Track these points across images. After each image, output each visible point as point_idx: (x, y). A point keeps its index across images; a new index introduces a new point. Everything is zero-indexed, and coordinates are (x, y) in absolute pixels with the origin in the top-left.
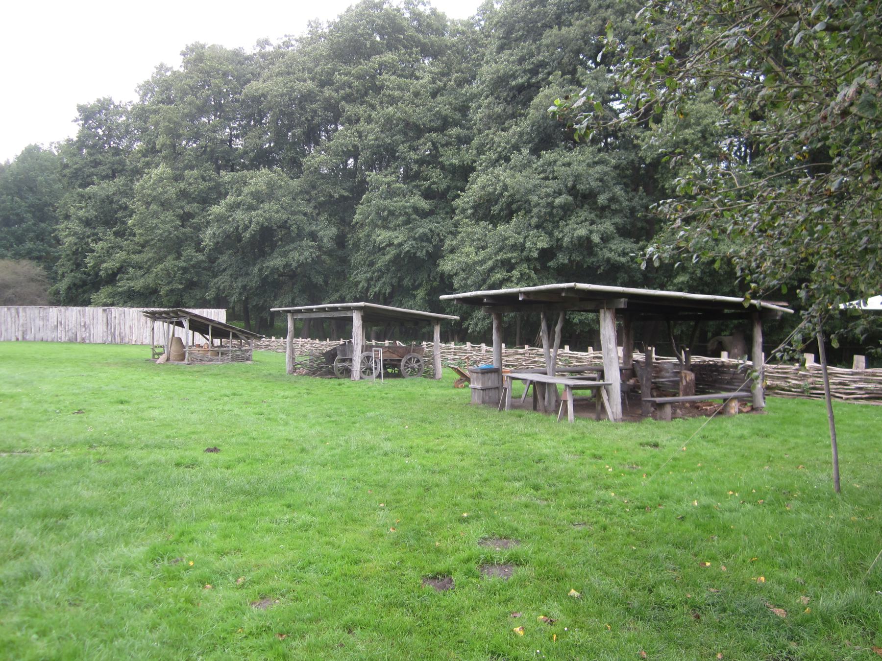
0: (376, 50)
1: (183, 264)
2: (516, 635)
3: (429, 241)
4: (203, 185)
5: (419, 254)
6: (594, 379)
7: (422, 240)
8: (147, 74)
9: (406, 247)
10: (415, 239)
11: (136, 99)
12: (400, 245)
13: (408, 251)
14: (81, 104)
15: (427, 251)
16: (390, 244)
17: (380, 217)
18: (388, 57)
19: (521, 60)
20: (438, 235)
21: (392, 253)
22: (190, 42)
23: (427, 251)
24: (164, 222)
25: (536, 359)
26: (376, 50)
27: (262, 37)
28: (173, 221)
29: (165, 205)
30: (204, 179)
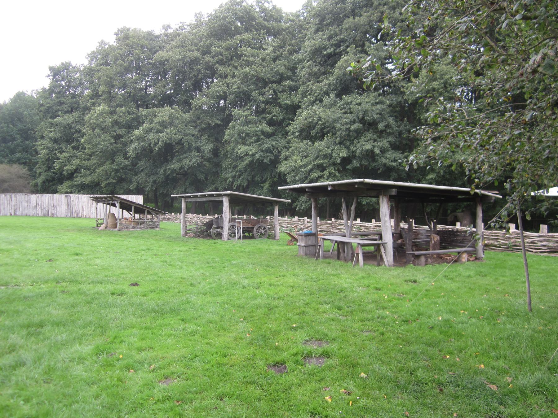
0: (238, 32)
1: (116, 167)
2: (326, 402)
3: (271, 152)
4: (128, 117)
5: (265, 161)
6: (376, 240)
7: (267, 152)
8: (93, 47)
9: (257, 156)
10: (262, 151)
11: (86, 63)
12: (253, 155)
13: (258, 159)
14: (52, 66)
15: (270, 159)
16: (247, 155)
17: (241, 137)
18: (246, 36)
19: (330, 38)
20: (277, 148)
21: (248, 160)
22: (120, 27)
23: (270, 159)
24: (104, 141)
25: (339, 227)
26: (238, 32)
27: (166, 23)
28: (109, 140)
29: (105, 130)
30: (129, 113)
